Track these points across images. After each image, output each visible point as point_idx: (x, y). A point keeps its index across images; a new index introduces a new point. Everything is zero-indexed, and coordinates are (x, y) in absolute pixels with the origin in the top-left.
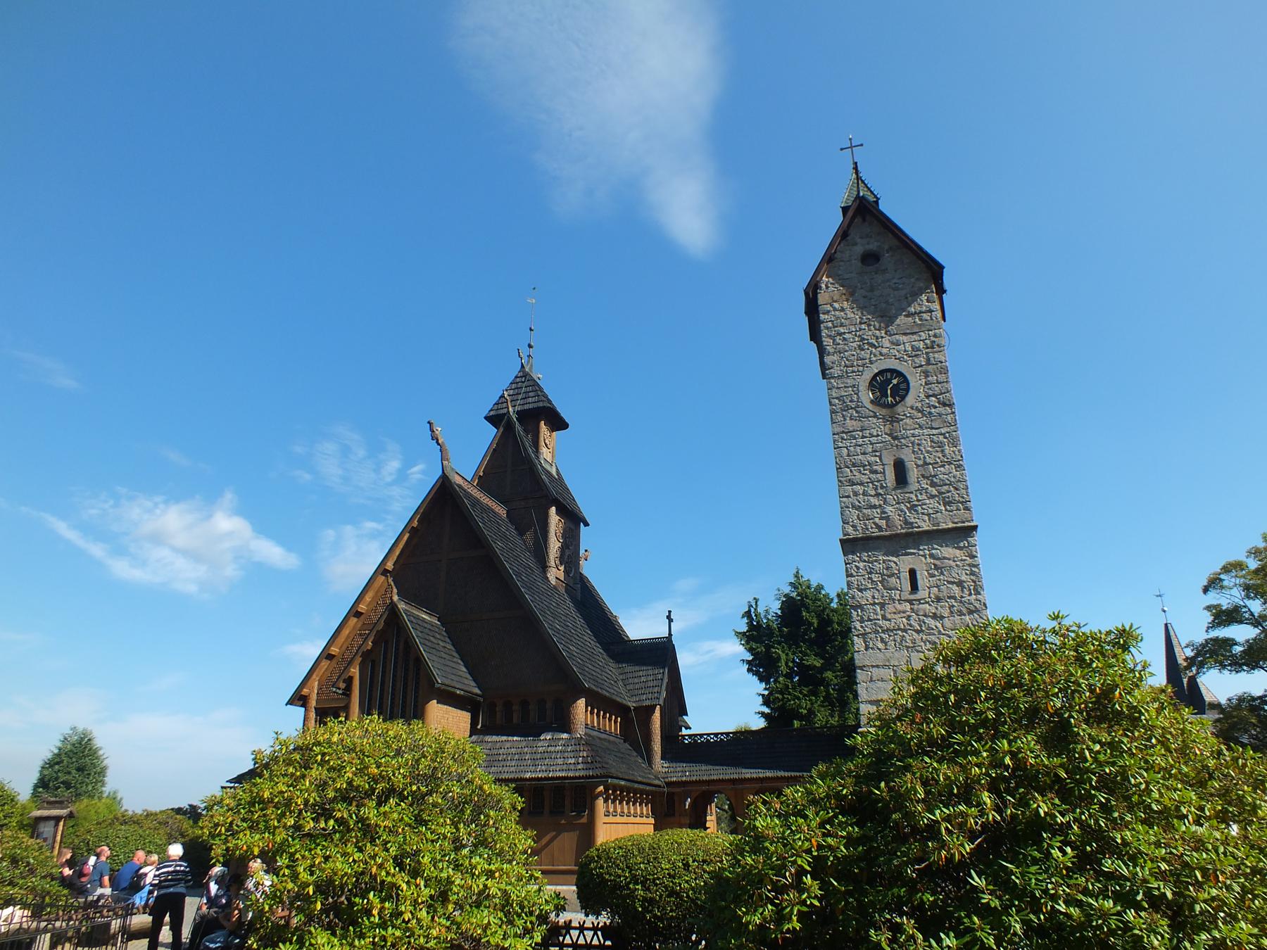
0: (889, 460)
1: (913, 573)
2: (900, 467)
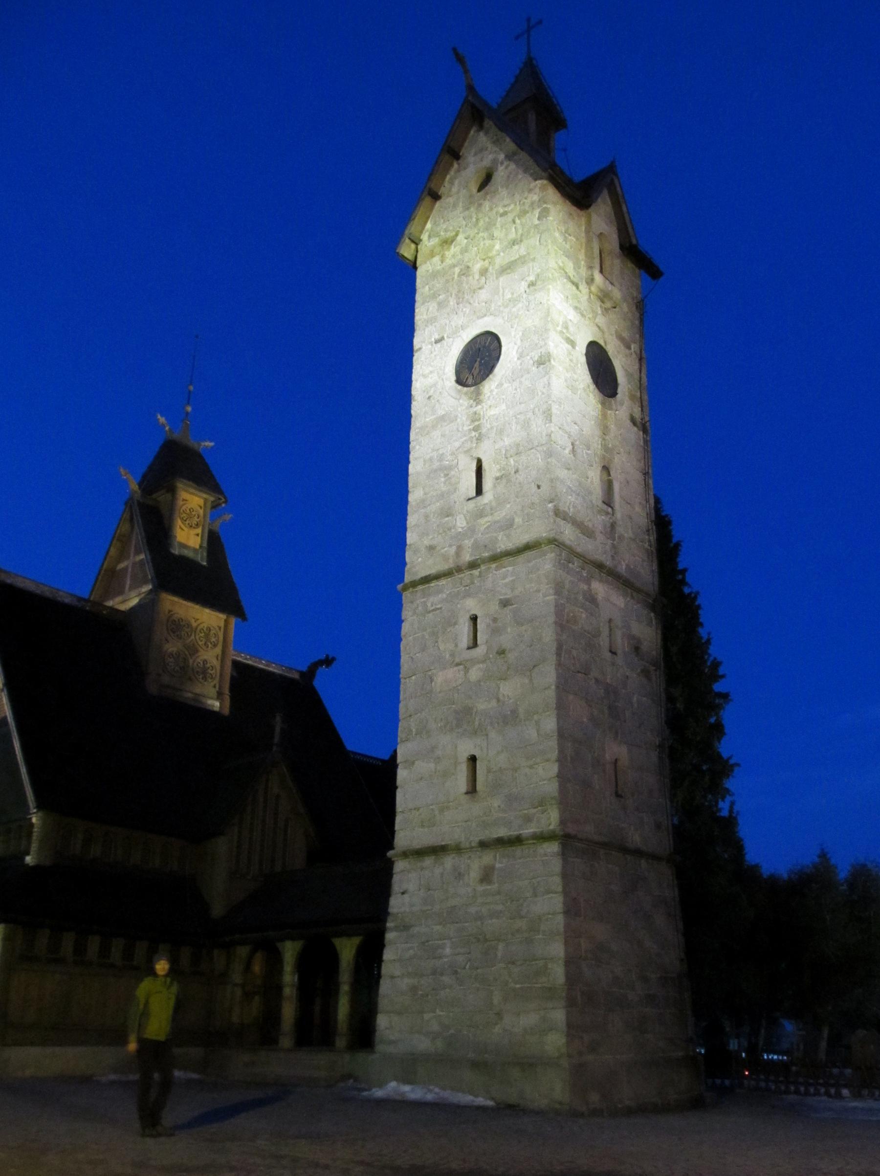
1: (474, 619)
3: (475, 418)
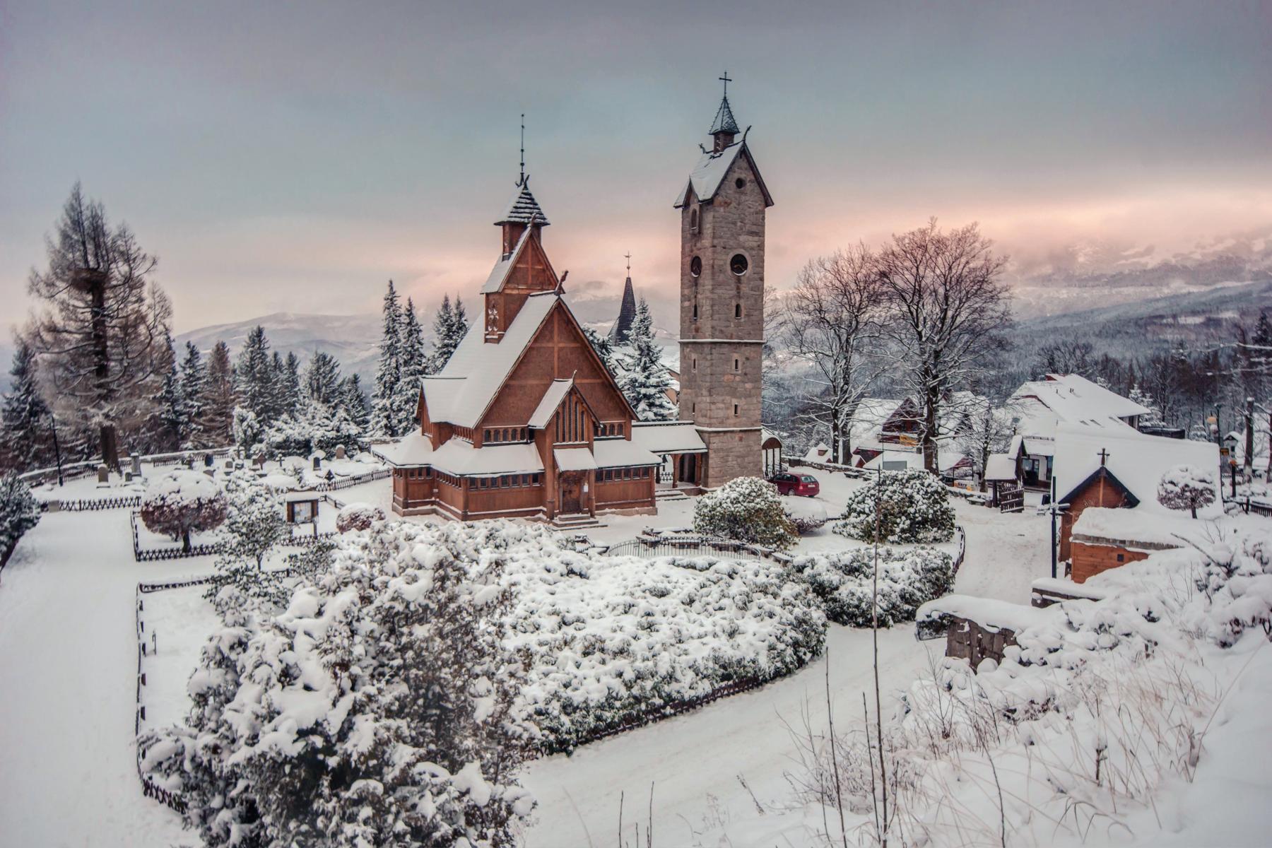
0: (734, 303)
2: (738, 307)
3: (738, 288)
